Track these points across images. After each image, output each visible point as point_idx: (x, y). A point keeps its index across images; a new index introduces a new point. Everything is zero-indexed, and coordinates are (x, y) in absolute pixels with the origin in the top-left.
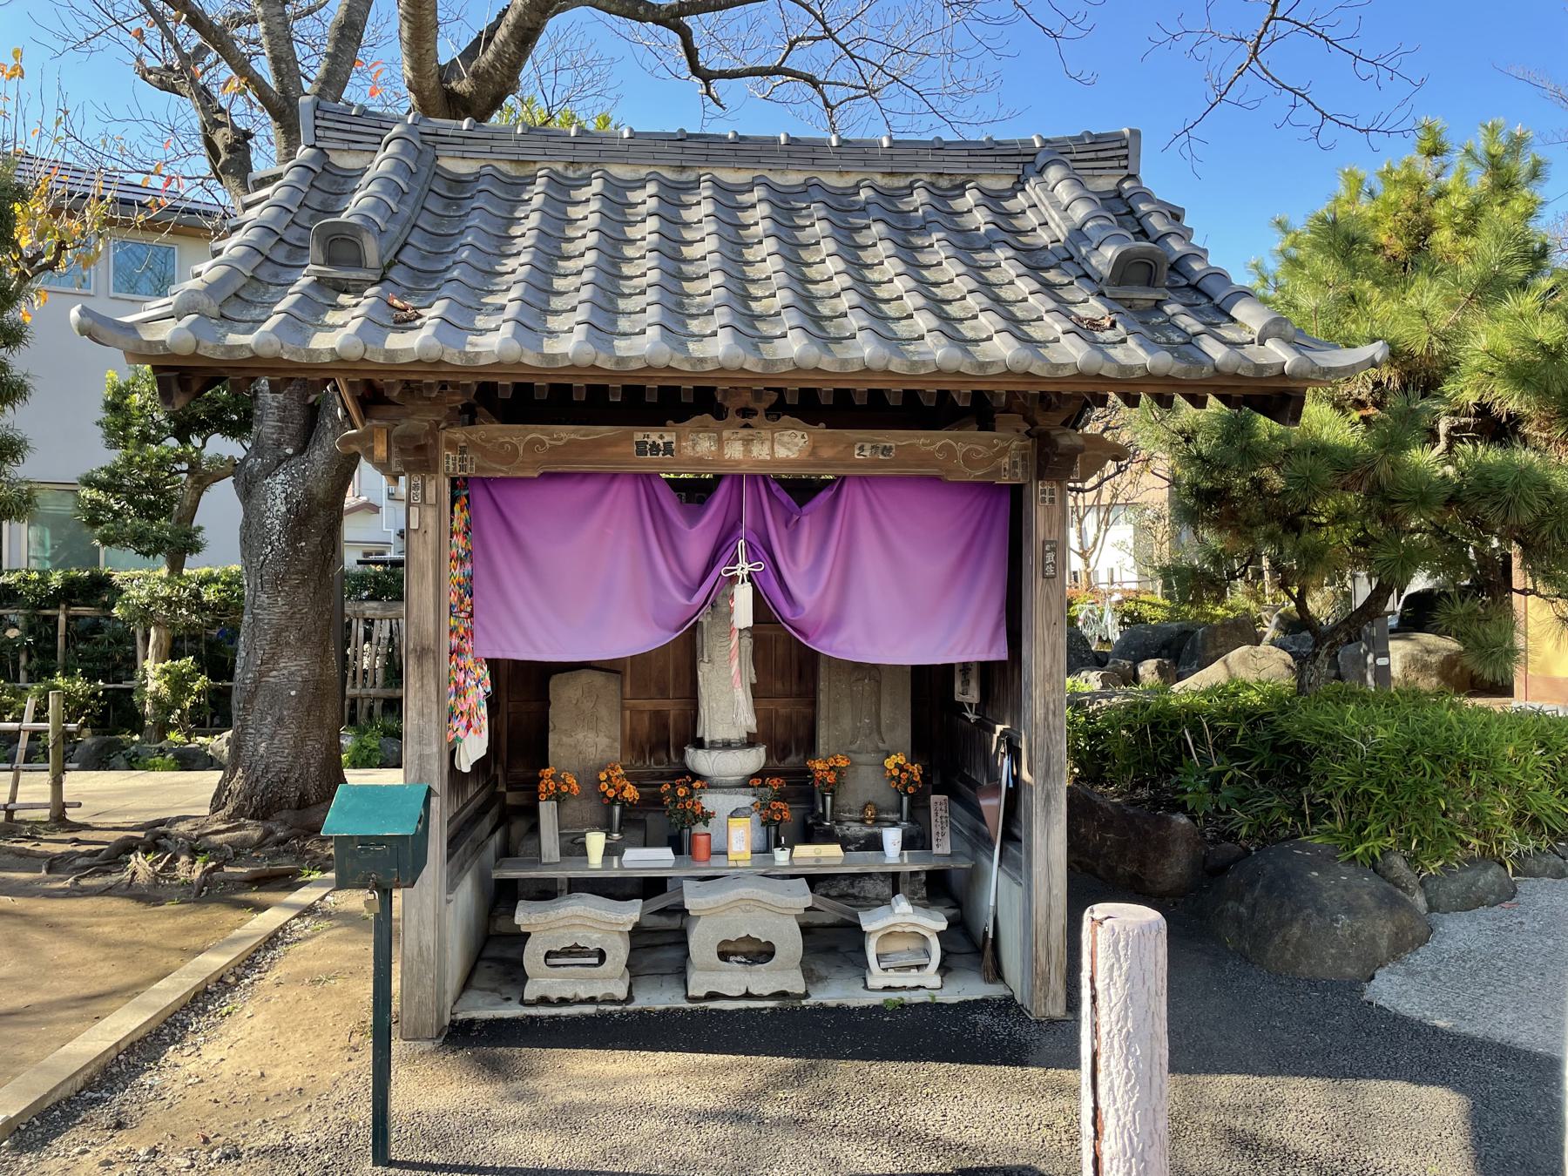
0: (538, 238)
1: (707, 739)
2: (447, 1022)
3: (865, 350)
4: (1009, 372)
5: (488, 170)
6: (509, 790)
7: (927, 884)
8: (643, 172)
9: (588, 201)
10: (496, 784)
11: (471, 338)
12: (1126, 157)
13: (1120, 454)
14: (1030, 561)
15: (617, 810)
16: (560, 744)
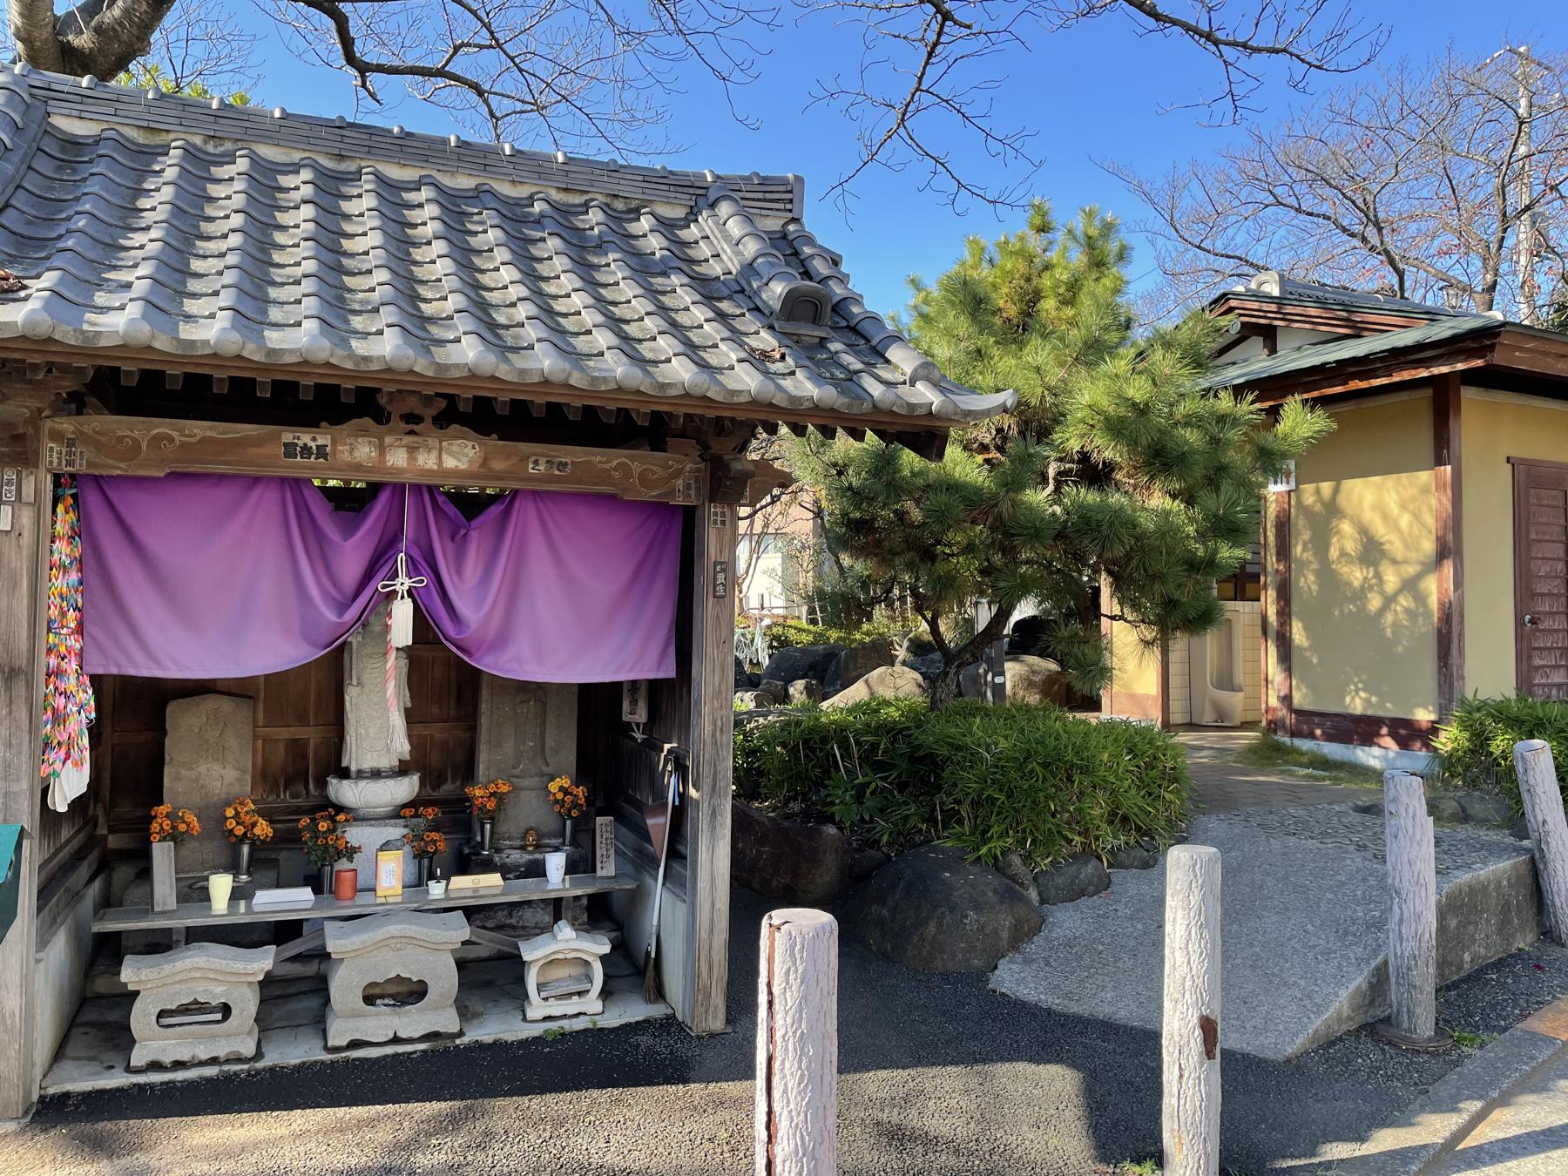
0: (173, 214)
1: (353, 768)
2: (35, 1098)
3: (545, 361)
4: (687, 395)
5: (112, 134)
6: (112, 830)
7: (589, 908)
8: (296, 156)
9: (231, 179)
10: (96, 826)
11: (88, 316)
12: (791, 201)
13: (785, 481)
14: (702, 581)
15: (246, 849)
16: (178, 778)
